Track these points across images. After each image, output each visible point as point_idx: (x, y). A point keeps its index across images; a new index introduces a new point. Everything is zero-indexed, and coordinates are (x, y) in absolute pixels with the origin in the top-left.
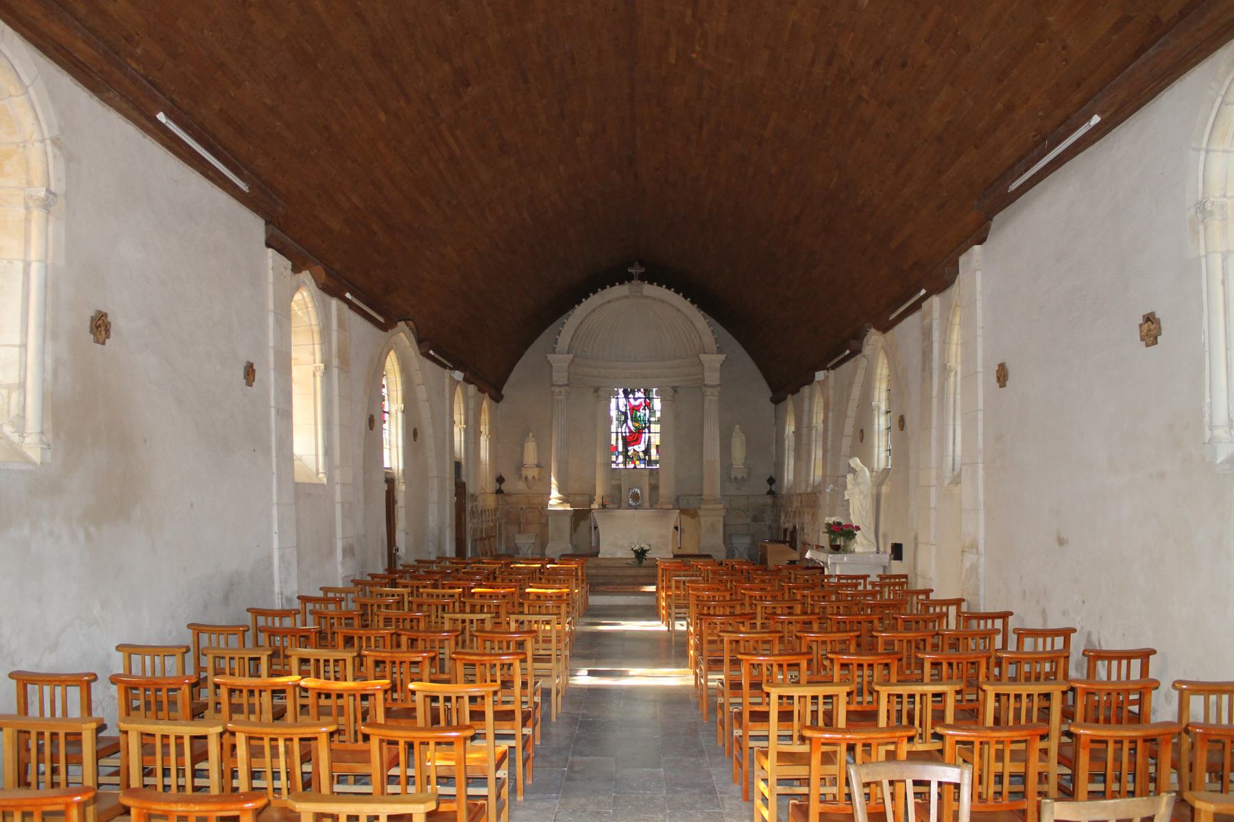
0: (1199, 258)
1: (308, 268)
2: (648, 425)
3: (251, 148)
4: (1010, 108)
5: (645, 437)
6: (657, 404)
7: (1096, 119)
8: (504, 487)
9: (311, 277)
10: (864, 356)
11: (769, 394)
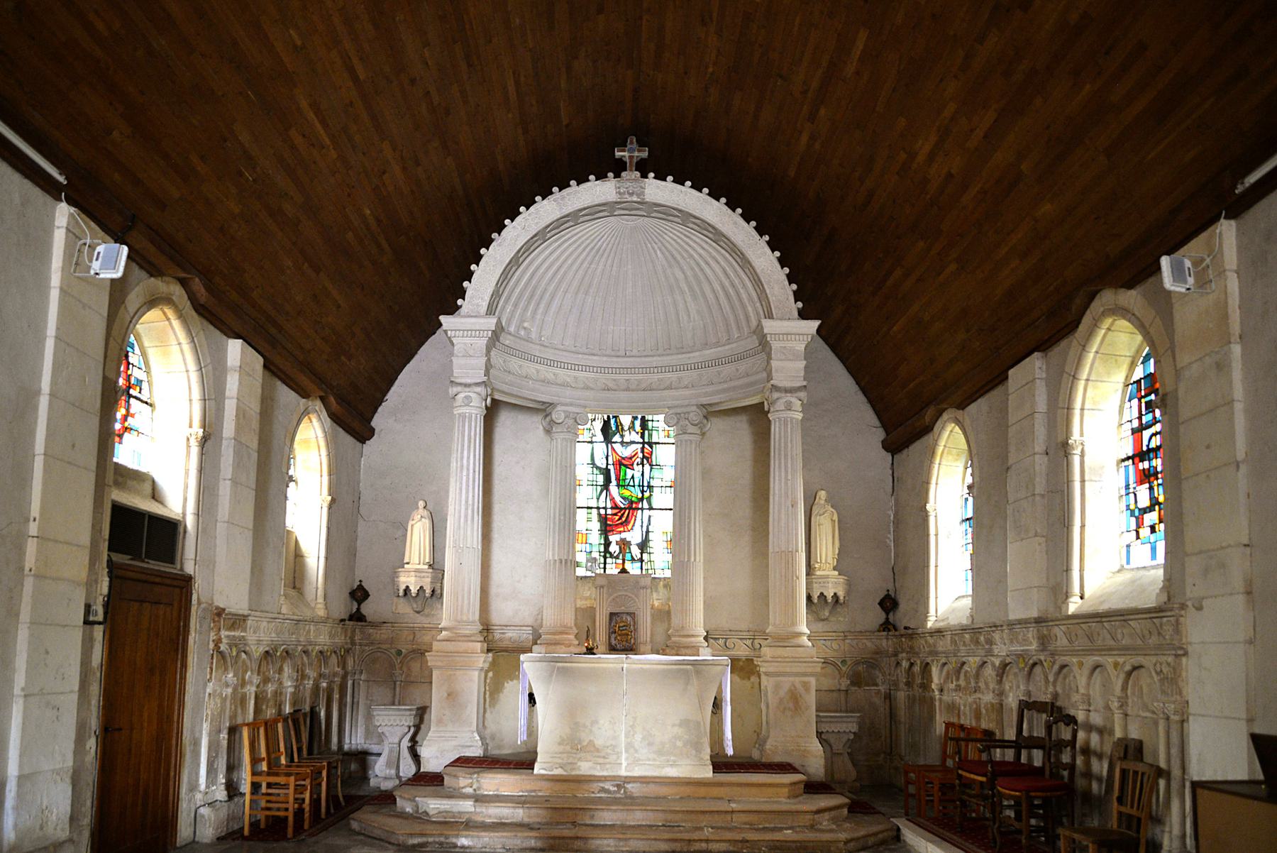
2: (647, 495)
6: (665, 455)
11: (880, 434)
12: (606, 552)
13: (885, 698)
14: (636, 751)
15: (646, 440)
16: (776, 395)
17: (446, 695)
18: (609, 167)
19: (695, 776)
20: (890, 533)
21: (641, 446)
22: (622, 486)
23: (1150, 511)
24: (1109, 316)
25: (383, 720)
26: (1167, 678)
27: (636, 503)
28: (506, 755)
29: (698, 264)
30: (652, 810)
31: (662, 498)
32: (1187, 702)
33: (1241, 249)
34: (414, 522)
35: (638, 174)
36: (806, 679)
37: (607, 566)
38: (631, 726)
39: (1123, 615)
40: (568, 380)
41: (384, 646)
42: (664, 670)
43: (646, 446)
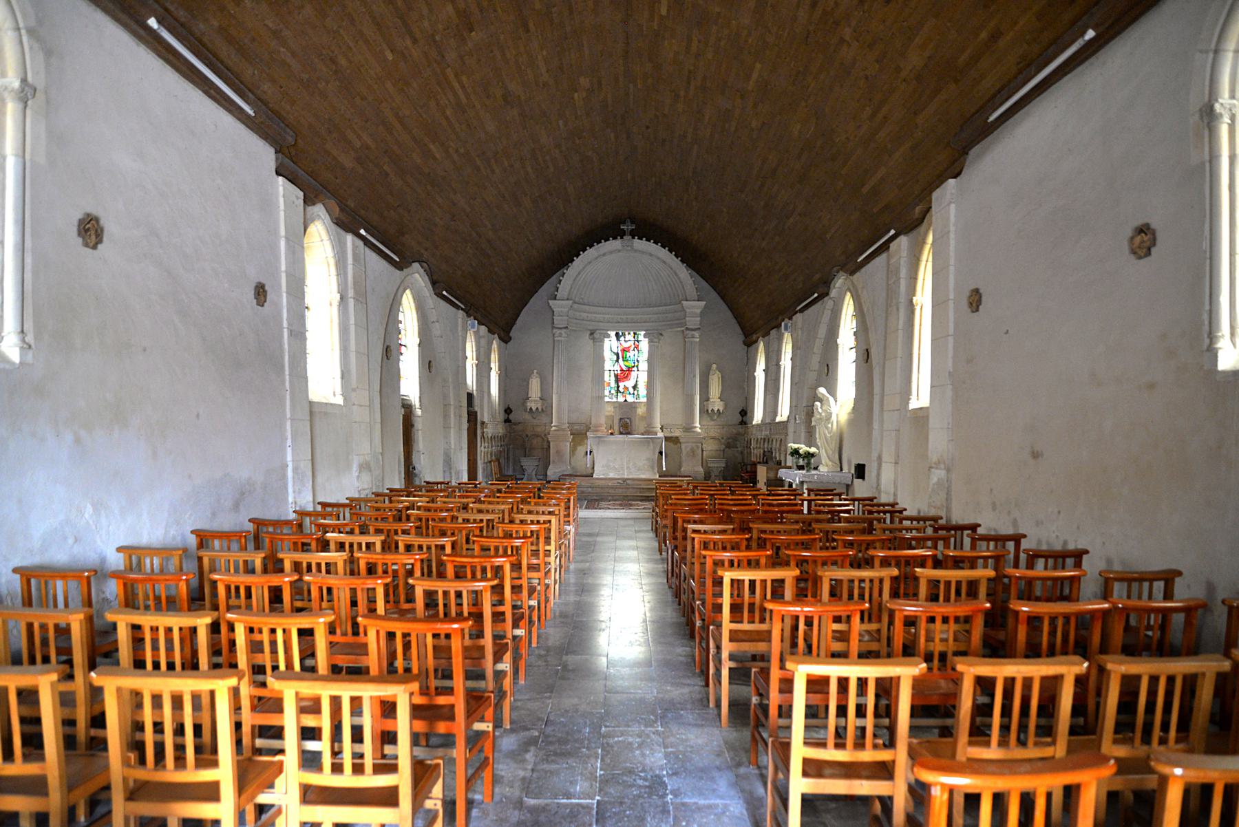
0: (1203, 164)
1: (321, 201)
2: (636, 364)
3: (256, 72)
4: (995, 36)
5: (634, 374)
7: (1090, 34)
8: (512, 417)
9: (325, 211)
10: (831, 298)
11: (742, 338)
12: (618, 391)
31: (644, 366)
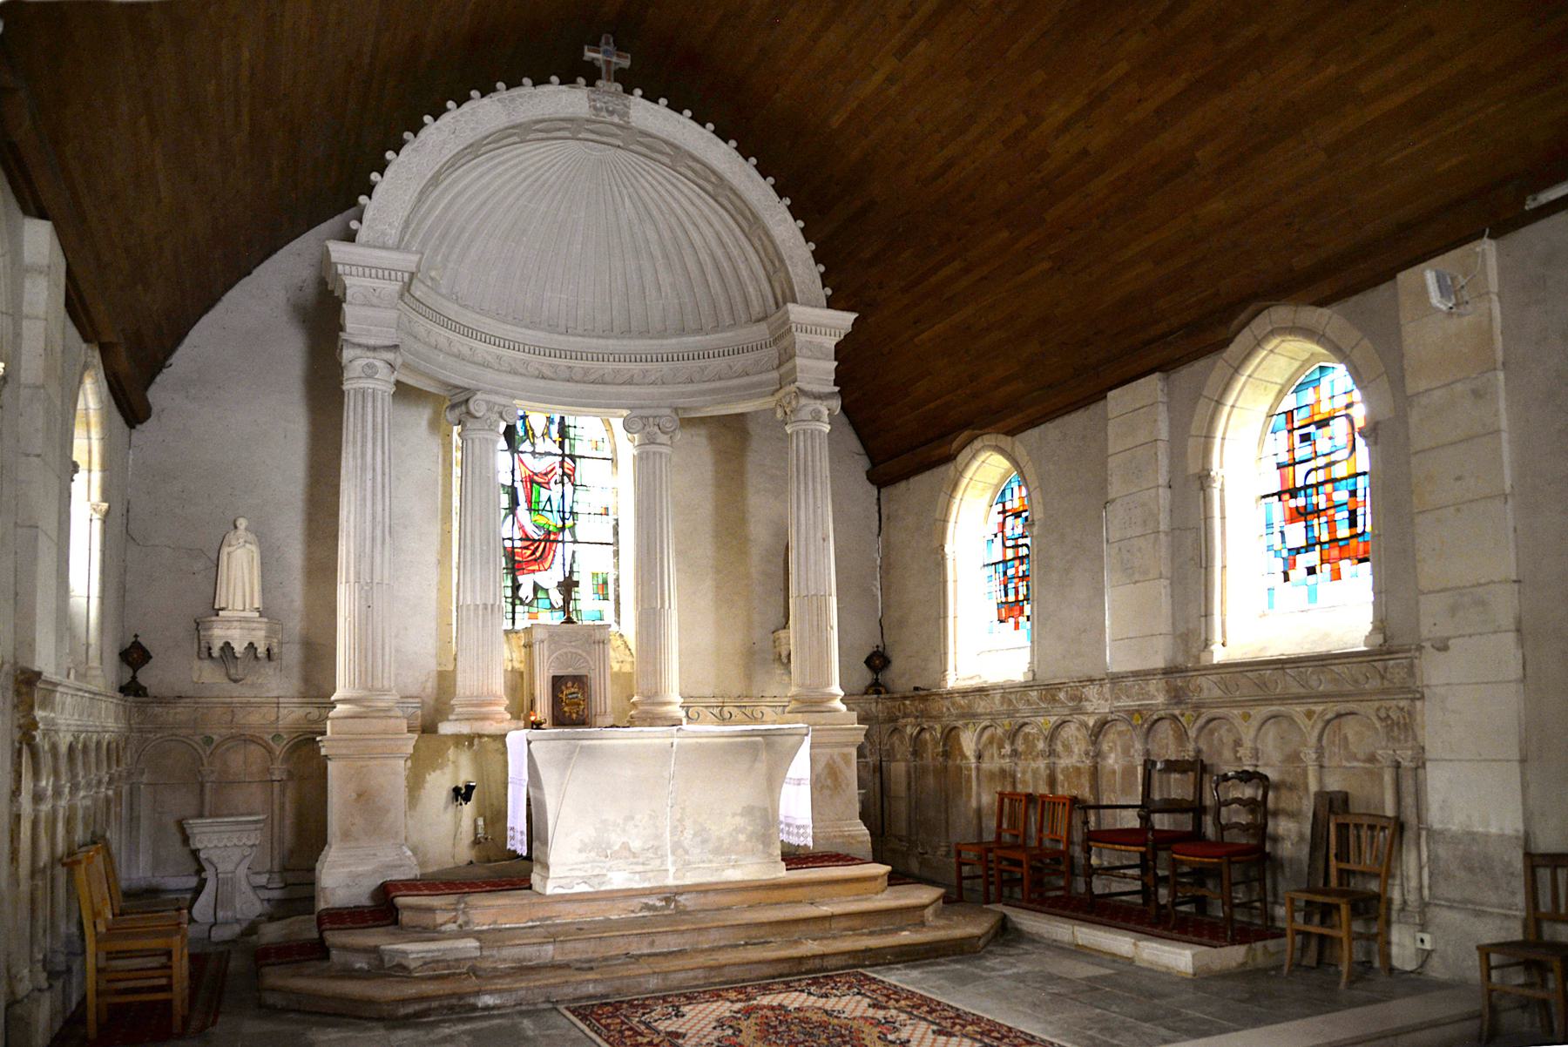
2: (569, 523)
8: (146, 676)
11: (863, 464)
13: (874, 772)
14: (687, 852)
15: (567, 452)
16: (803, 401)
17: (354, 796)
18: (575, 71)
19: (765, 877)
20: (876, 579)
21: (560, 458)
22: (535, 510)
23: (1307, 552)
24: (1279, 334)
25: (210, 841)
26: (1398, 723)
27: (555, 534)
28: (433, 873)
29: (681, 224)
30: (637, 934)
32: (1423, 748)
33: (1502, 271)
34: (231, 549)
35: (620, 88)
36: (846, 750)
37: (516, 615)
38: (678, 820)
39: (1322, 660)
40: (489, 358)
41: (183, 732)
42: (731, 744)
43: (567, 459)
